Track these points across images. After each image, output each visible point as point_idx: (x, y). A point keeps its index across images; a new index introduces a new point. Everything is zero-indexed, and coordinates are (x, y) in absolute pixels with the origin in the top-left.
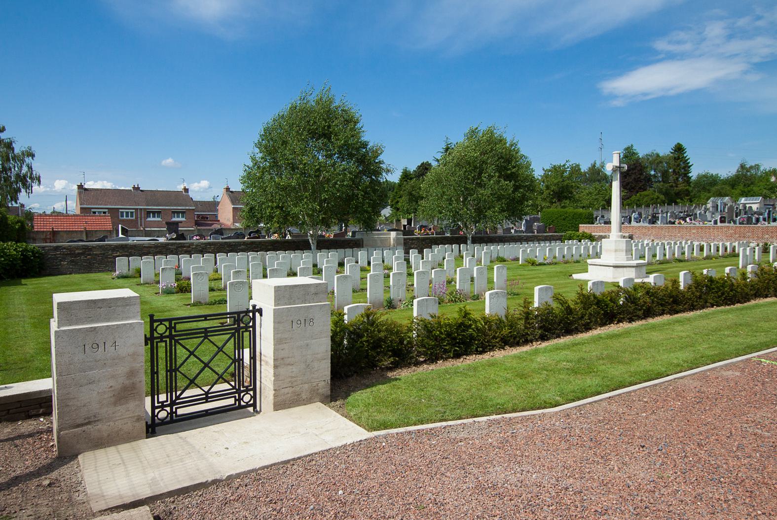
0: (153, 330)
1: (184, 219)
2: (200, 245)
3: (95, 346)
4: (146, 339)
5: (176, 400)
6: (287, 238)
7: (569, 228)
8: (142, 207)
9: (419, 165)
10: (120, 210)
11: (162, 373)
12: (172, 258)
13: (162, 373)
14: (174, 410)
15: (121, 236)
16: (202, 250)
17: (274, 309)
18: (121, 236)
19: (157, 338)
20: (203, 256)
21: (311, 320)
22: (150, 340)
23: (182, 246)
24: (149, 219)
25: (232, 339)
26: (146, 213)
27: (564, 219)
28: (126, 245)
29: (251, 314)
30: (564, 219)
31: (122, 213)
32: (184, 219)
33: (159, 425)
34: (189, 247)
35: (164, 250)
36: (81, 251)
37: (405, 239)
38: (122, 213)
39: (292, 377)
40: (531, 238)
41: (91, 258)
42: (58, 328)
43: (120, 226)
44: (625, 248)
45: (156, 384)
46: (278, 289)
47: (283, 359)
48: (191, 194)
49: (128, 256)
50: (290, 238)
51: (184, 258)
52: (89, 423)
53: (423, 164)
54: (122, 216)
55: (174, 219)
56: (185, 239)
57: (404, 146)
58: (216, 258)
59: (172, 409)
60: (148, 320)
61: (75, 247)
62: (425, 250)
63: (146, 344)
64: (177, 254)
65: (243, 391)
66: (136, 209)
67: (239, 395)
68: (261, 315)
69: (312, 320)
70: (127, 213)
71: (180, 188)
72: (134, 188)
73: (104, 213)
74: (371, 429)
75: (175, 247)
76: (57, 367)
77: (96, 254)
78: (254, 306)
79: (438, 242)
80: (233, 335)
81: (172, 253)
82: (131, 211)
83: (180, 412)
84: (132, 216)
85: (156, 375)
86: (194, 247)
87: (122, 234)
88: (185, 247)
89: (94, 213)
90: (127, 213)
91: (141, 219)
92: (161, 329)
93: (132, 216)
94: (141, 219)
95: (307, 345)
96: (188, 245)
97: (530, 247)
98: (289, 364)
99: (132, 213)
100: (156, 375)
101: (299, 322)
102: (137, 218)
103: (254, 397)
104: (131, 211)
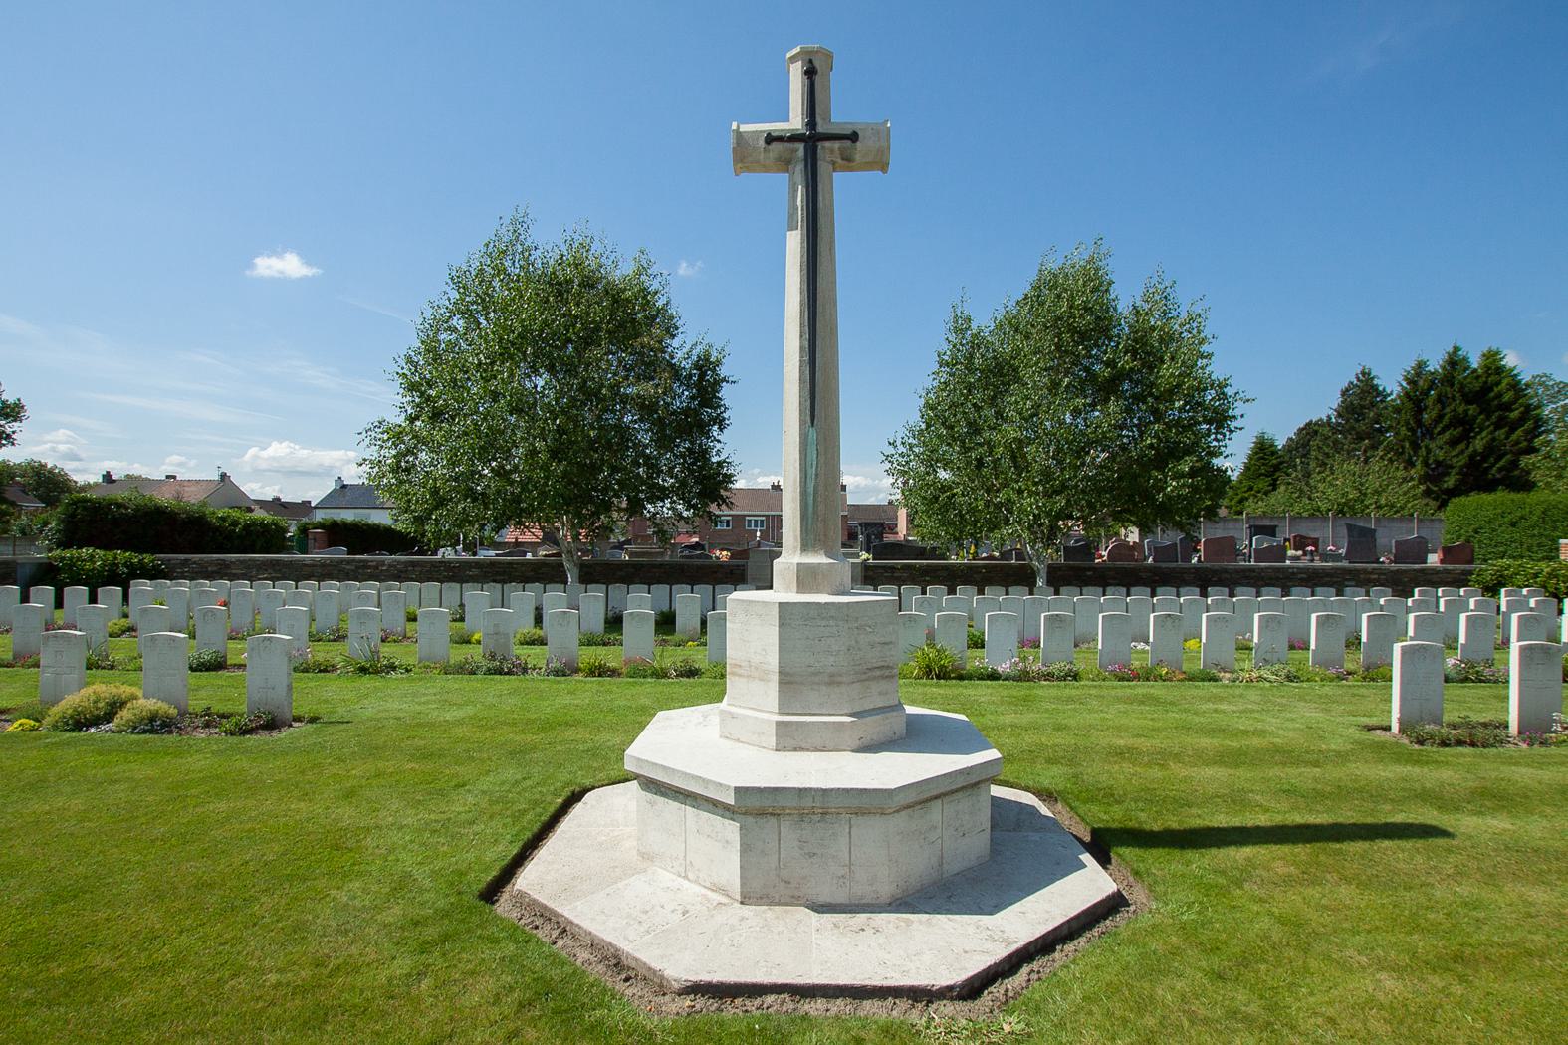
2: (395, 566)
7: (1529, 550)
8: (773, 513)
9: (1302, 426)
10: (747, 518)
20: (924, 593)
27: (1513, 525)
28: (277, 561)
30: (1513, 525)
31: (750, 521)
35: (336, 572)
36: (215, 569)
38: (750, 521)
40: (1328, 575)
44: (773, 660)
53: (1309, 424)
54: (749, 526)
57: (1273, 387)
58: (671, 590)
61: (207, 562)
66: (767, 516)
70: (756, 521)
72: (773, 486)
75: (353, 568)
76: (825, 722)
82: (755, 518)
84: (728, 526)
86: (385, 568)
90: (756, 521)
91: (773, 531)
96: (375, 564)
97: (1372, 605)
99: (762, 521)
102: (767, 528)
104: (755, 518)
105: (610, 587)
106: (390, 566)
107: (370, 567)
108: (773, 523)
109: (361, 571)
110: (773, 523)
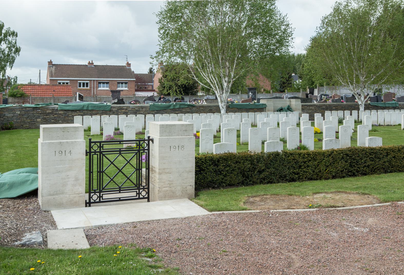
0: (90, 147)
1: (126, 89)
3: (60, 152)
4: (87, 153)
5: (102, 190)
6: (203, 104)
10: (79, 81)
11: (95, 174)
12: (114, 117)
13: (95, 174)
14: (101, 195)
15: (78, 100)
16: (136, 112)
17: (159, 138)
18: (78, 100)
19: (93, 152)
21: (183, 147)
22: (89, 153)
23: (121, 108)
24: (100, 89)
25: (136, 156)
26: (98, 83)
29: (147, 142)
31: (80, 83)
32: (126, 89)
33: (93, 203)
34: (127, 109)
36: (50, 111)
37: (302, 106)
38: (80, 83)
39: (170, 181)
41: (57, 117)
42: (43, 141)
43: (78, 93)
45: (91, 177)
46: (162, 126)
47: (164, 169)
48: (133, 68)
49: (82, 115)
50: (205, 103)
51: (122, 117)
52: (57, 194)
55: (119, 89)
56: (124, 103)
58: (344, 112)
59: (100, 195)
60: (88, 141)
62: (315, 114)
63: (86, 155)
64: (118, 114)
65: (141, 189)
67: (139, 191)
68: (153, 143)
69: (183, 147)
70: (84, 84)
71: (124, 64)
72: (89, 63)
73: (67, 83)
74: (211, 211)
77: (60, 114)
78: (149, 137)
79: (334, 108)
80: (136, 153)
81: (114, 113)
83: (105, 197)
85: (91, 174)
86: (130, 109)
87: (79, 99)
88: (123, 109)
89: (60, 83)
90: (84, 84)
91: (94, 89)
92: (95, 148)
93: (87, 86)
94: (94, 89)
95: (180, 162)
96: (126, 108)
98: (168, 173)
99: (87, 84)
100: (91, 174)
101: (175, 147)
103: (148, 193)
105: (345, 111)
106: (133, 108)
107: (123, 109)
108: (94, 85)
109: (120, 111)
110: (94, 85)
